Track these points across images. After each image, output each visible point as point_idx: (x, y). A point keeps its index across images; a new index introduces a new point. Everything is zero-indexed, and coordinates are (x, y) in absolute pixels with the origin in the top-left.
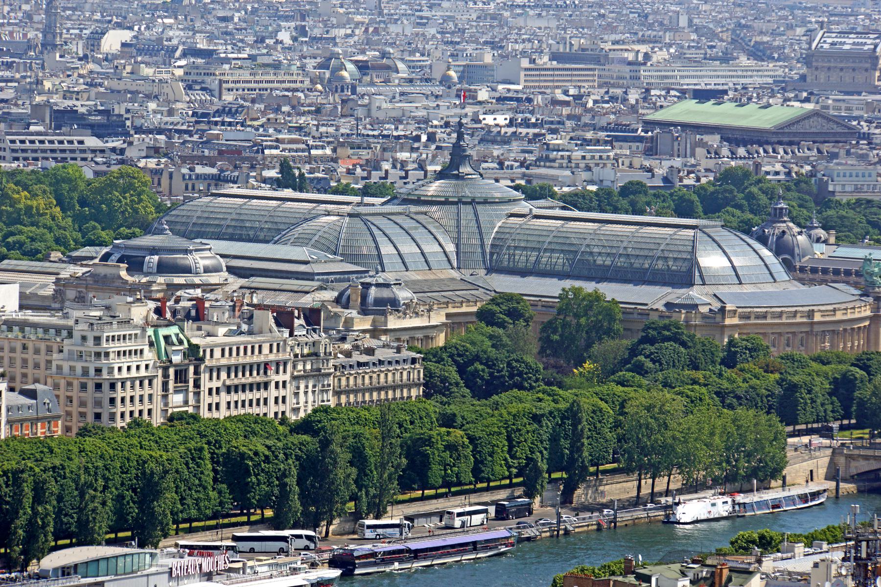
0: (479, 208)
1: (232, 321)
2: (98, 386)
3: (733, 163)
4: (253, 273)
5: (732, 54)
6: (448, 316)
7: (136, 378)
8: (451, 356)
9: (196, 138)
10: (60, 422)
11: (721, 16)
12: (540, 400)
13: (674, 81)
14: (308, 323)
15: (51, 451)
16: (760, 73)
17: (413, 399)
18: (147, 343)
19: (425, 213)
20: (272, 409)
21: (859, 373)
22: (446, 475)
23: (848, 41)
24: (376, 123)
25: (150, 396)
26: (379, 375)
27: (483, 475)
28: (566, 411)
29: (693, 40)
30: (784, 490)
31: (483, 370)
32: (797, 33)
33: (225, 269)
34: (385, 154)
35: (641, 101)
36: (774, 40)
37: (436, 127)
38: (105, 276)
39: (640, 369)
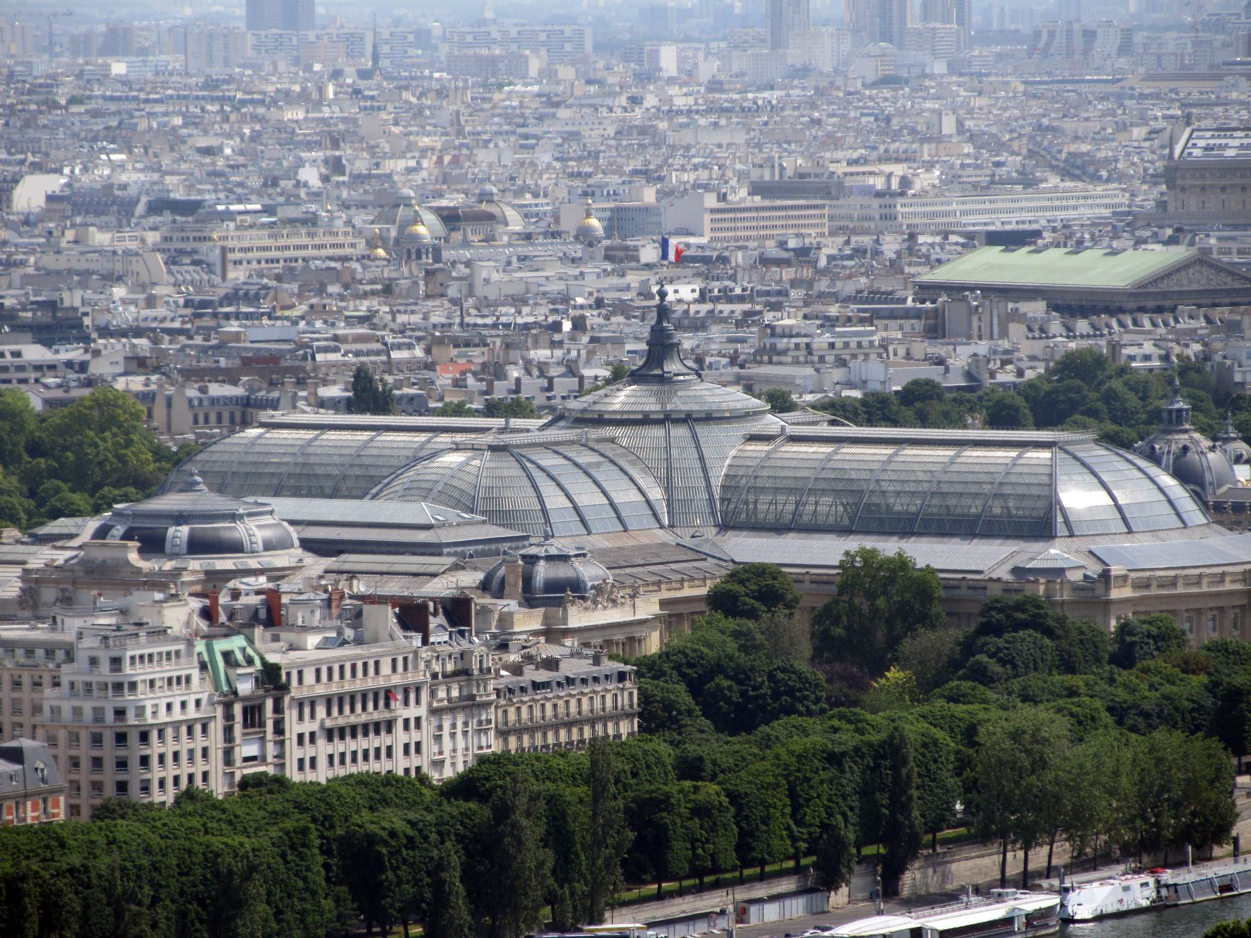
0: (701, 430)
1: (328, 623)
2: (121, 738)
3: (1073, 345)
4: (341, 547)
5: (1033, 174)
6: (663, 603)
7: (181, 722)
8: (677, 667)
10: (62, 799)
11: (1007, 114)
12: (836, 730)
13: (951, 219)
14: (452, 623)
15: (63, 845)
16: (1089, 202)
17: (624, 738)
18: (196, 664)
19: (612, 440)
20: (399, 765)
22: (696, 856)
23: (1231, 142)
24: (485, 304)
26: (567, 702)
27: (754, 854)
28: (881, 746)
29: (968, 155)
30: (1236, 862)
31: (730, 688)
32: (1134, 137)
33: (297, 543)
34: (511, 352)
35: (905, 253)
36: (1099, 149)
37: (582, 307)
38: (104, 562)
39: (981, 676)
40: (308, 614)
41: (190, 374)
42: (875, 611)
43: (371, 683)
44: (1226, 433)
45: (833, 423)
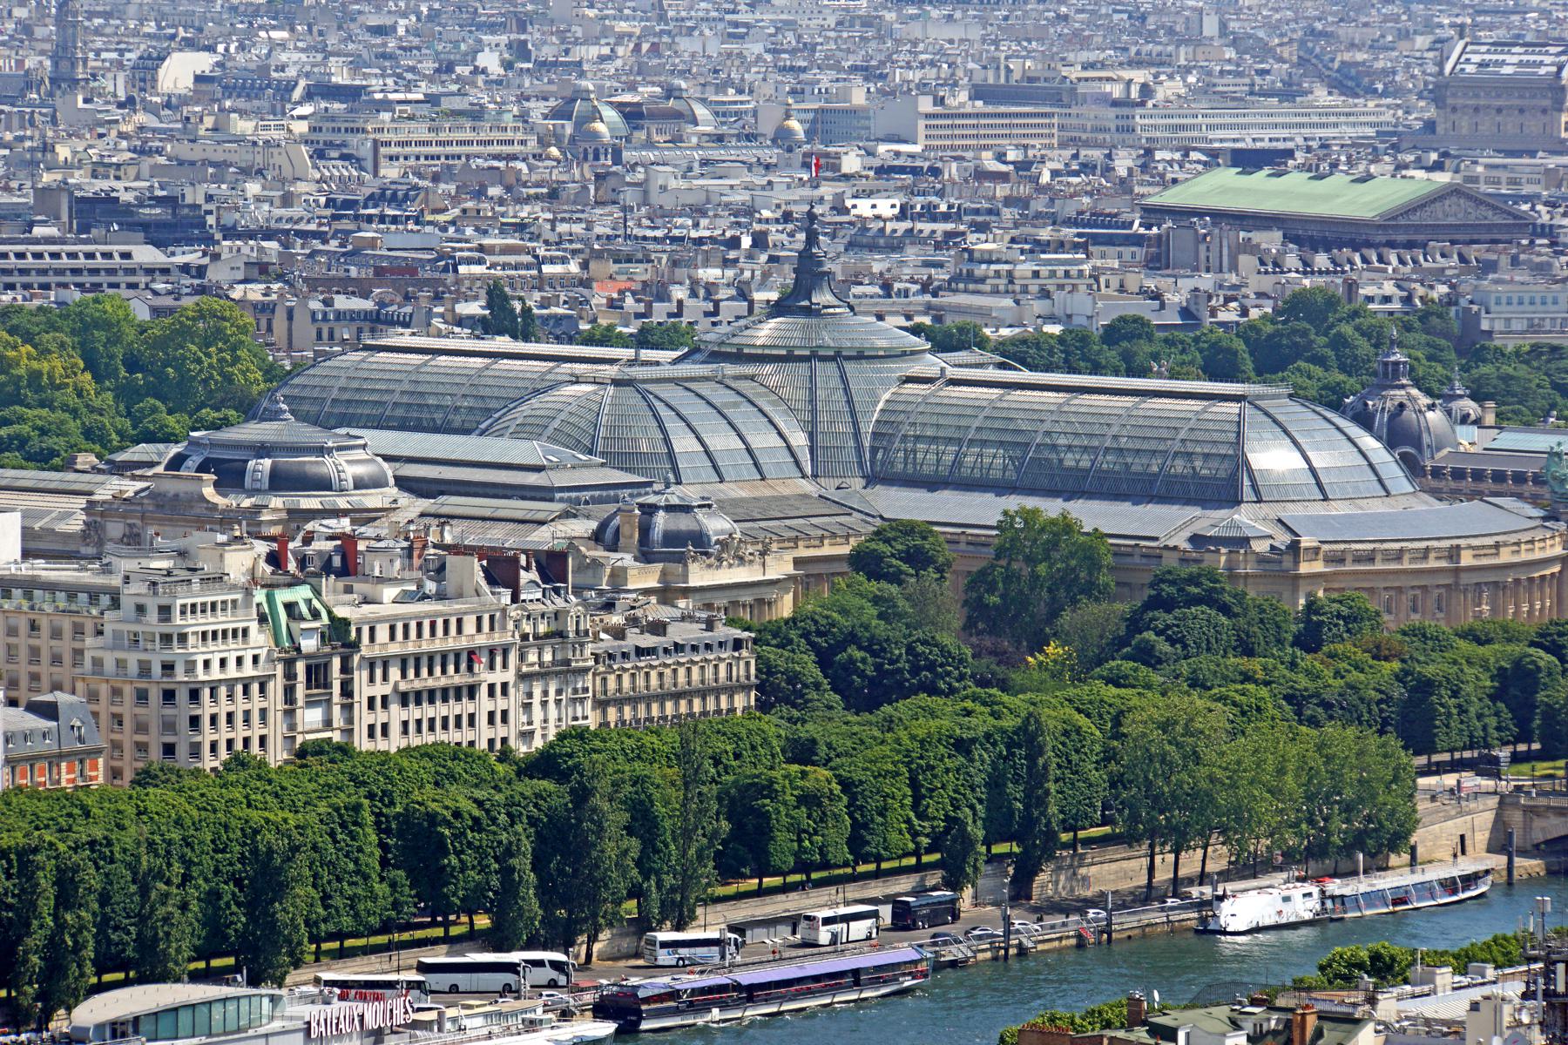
0: (849, 367)
1: (407, 574)
2: (169, 696)
3: (1307, 282)
4: (442, 488)
6: (797, 562)
7: (237, 680)
8: (806, 635)
9: (333, 245)
10: (101, 761)
11: (1278, 16)
12: (968, 713)
13: (1195, 134)
14: (546, 578)
16: (1352, 119)
17: (739, 713)
18: (255, 616)
19: (752, 378)
24: (659, 215)
25: (263, 712)
26: (675, 671)
27: (868, 848)
29: (1229, 61)
30: (1413, 872)
31: (864, 660)
33: (392, 481)
36: (1376, 59)
37: (767, 221)
38: (176, 495)
40: (386, 563)
42: (1035, 577)
44: (1452, 389)
45: (1002, 366)
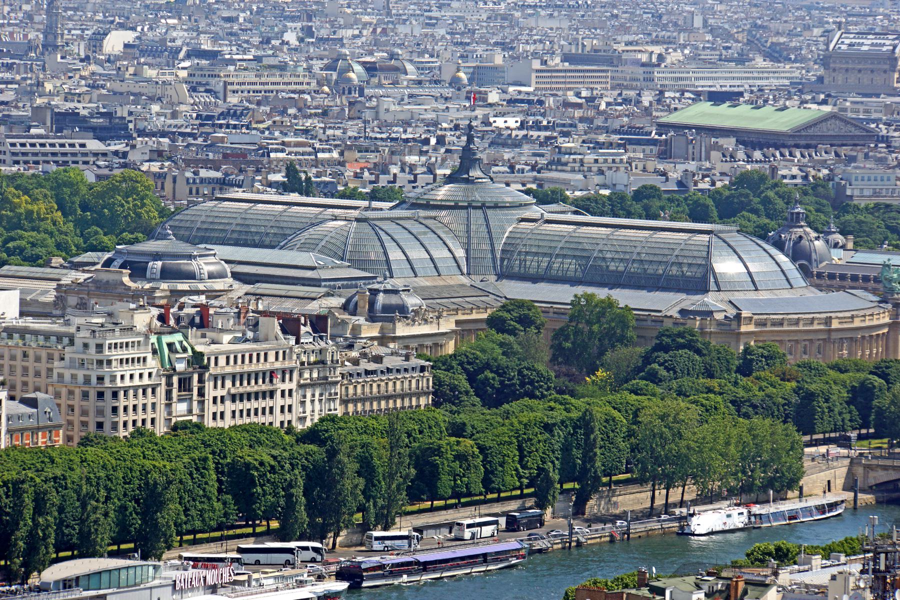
0: (490, 212)
1: (237, 328)
2: (101, 395)
3: (749, 167)
4: (258, 279)
5: (748, 55)
6: (458, 323)
7: (139, 386)
8: (461, 364)
9: (200, 141)
10: (61, 431)
11: (736, 17)
12: (552, 409)
13: (688, 82)
15: (52, 461)
16: (776, 75)
17: (422, 408)
18: (150, 350)
19: (435, 218)
20: (278, 418)
21: (878, 381)
22: (456, 486)
23: (866, 42)
24: (384, 125)
25: (154, 405)
26: (387, 384)
27: (493, 485)
29: (708, 41)
30: (800, 501)
31: (493, 379)
32: (814, 34)
33: (229, 275)
34: (394, 157)
35: (655, 103)
36: (791, 41)
37: (445, 129)
38: (108, 282)
41: (188, 163)
42: (591, 332)
43: (261, 367)
45: (576, 213)
